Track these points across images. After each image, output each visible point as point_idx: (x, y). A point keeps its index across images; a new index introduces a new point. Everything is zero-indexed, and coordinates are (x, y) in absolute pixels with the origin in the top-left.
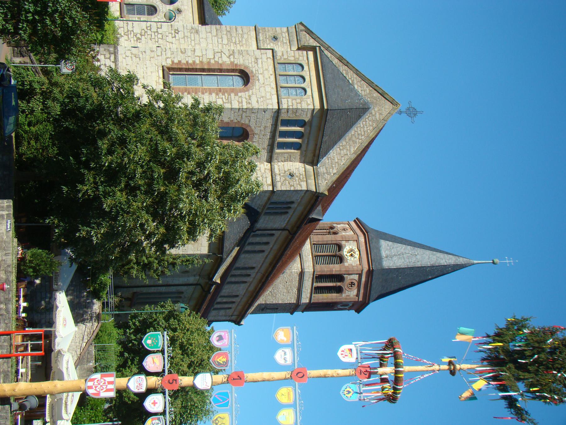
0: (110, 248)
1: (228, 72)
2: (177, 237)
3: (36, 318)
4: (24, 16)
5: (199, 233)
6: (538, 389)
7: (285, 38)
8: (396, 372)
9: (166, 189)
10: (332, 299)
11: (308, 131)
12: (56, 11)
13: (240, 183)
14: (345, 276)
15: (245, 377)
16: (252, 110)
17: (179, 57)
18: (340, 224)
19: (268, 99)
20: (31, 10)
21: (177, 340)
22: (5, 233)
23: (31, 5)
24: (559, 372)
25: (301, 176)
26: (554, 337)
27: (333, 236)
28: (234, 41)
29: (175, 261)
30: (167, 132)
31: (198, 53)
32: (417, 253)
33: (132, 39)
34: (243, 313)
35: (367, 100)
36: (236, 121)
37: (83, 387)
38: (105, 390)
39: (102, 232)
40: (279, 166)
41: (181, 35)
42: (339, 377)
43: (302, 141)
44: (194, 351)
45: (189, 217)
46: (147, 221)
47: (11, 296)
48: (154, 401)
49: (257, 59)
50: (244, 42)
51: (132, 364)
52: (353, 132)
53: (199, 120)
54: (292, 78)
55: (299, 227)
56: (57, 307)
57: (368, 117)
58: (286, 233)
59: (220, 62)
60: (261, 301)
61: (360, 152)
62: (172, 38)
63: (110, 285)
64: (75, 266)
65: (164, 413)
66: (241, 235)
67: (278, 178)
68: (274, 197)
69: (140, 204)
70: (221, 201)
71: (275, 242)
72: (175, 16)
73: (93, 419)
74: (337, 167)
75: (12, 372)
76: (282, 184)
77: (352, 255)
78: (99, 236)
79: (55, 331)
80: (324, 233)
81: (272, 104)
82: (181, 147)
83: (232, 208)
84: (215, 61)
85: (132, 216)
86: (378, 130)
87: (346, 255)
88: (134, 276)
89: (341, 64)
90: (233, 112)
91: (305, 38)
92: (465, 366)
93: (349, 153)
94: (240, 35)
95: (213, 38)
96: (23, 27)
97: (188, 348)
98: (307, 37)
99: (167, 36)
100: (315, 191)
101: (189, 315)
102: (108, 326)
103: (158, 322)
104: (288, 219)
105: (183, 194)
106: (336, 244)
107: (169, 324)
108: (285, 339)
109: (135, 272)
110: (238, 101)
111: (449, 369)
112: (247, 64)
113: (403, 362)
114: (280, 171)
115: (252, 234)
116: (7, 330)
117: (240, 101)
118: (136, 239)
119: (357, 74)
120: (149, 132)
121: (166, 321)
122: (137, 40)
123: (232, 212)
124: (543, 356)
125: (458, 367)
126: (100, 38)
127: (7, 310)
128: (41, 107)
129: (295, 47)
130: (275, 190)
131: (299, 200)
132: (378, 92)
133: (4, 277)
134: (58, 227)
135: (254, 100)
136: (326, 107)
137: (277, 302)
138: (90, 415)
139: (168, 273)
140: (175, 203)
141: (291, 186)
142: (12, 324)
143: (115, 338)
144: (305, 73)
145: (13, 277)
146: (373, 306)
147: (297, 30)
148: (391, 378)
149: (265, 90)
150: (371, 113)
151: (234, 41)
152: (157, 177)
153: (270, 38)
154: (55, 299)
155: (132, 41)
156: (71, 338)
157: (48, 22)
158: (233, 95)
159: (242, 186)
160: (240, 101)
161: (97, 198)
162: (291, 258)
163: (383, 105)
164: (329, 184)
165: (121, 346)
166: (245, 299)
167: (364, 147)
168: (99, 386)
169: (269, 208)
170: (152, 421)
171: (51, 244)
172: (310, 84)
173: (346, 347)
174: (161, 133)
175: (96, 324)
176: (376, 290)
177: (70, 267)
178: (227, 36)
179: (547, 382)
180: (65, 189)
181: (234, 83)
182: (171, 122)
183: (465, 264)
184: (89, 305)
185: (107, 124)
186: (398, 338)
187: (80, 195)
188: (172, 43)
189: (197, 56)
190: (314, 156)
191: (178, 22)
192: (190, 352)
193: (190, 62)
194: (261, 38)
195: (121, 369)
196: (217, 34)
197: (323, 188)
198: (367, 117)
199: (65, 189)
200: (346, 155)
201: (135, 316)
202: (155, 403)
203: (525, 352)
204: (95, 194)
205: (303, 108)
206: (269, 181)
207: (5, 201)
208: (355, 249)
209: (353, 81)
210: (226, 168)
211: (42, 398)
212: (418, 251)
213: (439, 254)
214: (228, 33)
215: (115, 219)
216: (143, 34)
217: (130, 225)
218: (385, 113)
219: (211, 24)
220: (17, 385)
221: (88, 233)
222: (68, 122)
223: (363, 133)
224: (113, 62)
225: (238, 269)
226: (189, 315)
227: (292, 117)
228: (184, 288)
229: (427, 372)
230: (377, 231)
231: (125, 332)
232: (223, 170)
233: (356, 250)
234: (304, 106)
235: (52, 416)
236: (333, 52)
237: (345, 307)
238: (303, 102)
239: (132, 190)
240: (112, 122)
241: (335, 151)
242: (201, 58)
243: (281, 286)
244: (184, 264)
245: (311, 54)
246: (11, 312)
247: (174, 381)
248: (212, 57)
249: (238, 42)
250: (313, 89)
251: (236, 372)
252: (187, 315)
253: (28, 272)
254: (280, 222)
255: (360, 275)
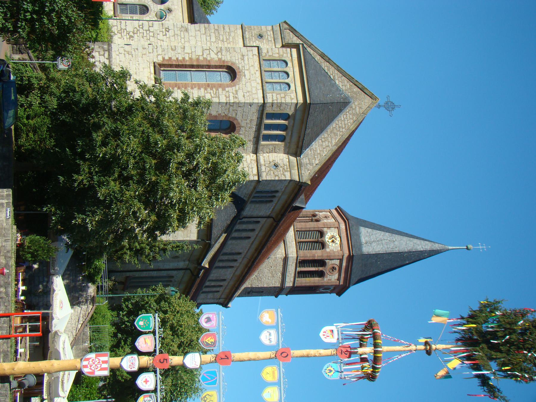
0: (104, 235)
1: (216, 68)
2: (168, 224)
3: (34, 300)
4: (22, 15)
5: (189, 220)
6: (509, 368)
7: (270, 36)
8: (375, 352)
9: (158, 179)
10: (315, 283)
11: (292, 124)
12: (53, 10)
13: (227, 173)
14: (327, 261)
15: (232, 357)
16: (239, 104)
17: (169, 54)
18: (322, 212)
19: (254, 94)
20: (30, 10)
21: (167, 322)
22: (4, 220)
23: (29, 5)
24: (529, 352)
25: (286, 167)
26: (525, 319)
27: (316, 223)
28: (221, 39)
29: (166, 247)
30: (158, 125)
31: (187, 50)
32: (394, 240)
33: (125, 37)
34: (230, 296)
35: (348, 95)
36: (223, 114)
37: (79, 366)
38: (99, 368)
39: (97, 219)
40: (264, 157)
41: (171, 33)
42: (321, 356)
43: (286, 134)
44: (184, 332)
45: (179, 206)
46: (139, 209)
47: (10, 280)
48: (146, 379)
49: (243, 56)
50: (231, 40)
51: (125, 344)
52: (334, 125)
53: (189, 114)
54: (277, 74)
55: (283, 215)
56: (54, 291)
57: (349, 111)
58: (271, 220)
59: (208, 59)
60: (247, 284)
61: (340, 144)
62: (163, 35)
63: (104, 270)
64: (71, 252)
65: (155, 391)
66: (229, 222)
67: (263, 168)
68: (260, 186)
69: (132, 193)
70: (210, 190)
71: (261, 229)
72: (166, 15)
73: (88, 396)
74: (319, 158)
75: (11, 352)
76: (267, 174)
77: (333, 241)
78: (94, 223)
79: (52, 313)
80: (307, 221)
81: (258, 99)
82: (171, 139)
83: (220, 196)
84: (204, 58)
85: (125, 204)
86: (358, 123)
87: (328, 241)
88: (127, 261)
89: (323, 61)
90: (220, 106)
91: (289, 36)
92: (440, 346)
93: (330, 145)
94: (227, 33)
95: (202, 36)
96: (22, 25)
97: (178, 329)
98: (291, 35)
99: (158, 34)
100: (298, 180)
101: (179, 298)
102: (102, 308)
103: (150, 305)
104: (273, 207)
105: (173, 184)
106: (319, 231)
107: (160, 306)
108: (270, 321)
109: (128, 258)
110: (226, 96)
111: (426, 349)
112: (234, 61)
113: (381, 342)
114: (265, 162)
115: (239, 221)
116: (7, 312)
117: (227, 95)
118: (128, 226)
119: (338, 70)
120: (141, 125)
121: (157, 304)
122: (130, 38)
123: (220, 200)
124: (514, 336)
125: (434, 347)
126: (94, 36)
127: (7, 294)
128: (39, 101)
129: (279, 45)
130: (260, 180)
131: (283, 189)
132: (358, 87)
133: (4, 262)
134: (55, 214)
135: (240, 94)
136: (308, 102)
137: (262, 286)
138: (85, 393)
139: (159, 258)
140: (166, 192)
141: (276, 176)
142: (12, 307)
143: (109, 320)
144: (289, 69)
145: (12, 262)
146: (353, 290)
147: (281, 28)
148: (371, 357)
149: (251, 85)
150: (352, 107)
151: (221, 39)
152: (149, 168)
153: (256, 36)
154: (52, 283)
155: (125, 39)
156: (68, 320)
157: (46, 21)
158: (220, 90)
159: (229, 176)
160: (227, 95)
161: (91, 187)
162: (276, 244)
163: (363, 99)
164: (311, 174)
165: (114, 327)
166: (232, 283)
167: (344, 139)
168: (94, 365)
169: (254, 197)
170: (144, 398)
171: (49, 231)
172: (293, 80)
173: (327, 328)
174: (153, 126)
175: (91, 306)
176: (356, 274)
177: (67, 252)
178: (215, 34)
179: (518, 362)
180: (61, 178)
181: (222, 79)
182: (162, 116)
183: (440, 250)
184: (84, 289)
185: (101, 118)
186: (377, 320)
187: (76, 185)
188: (163, 41)
189: (187, 53)
190: (298, 147)
191: (169, 20)
192: (180, 333)
193: (180, 58)
194: (247, 36)
195: (115, 349)
196: (205, 32)
197: (306, 177)
198: (348, 110)
199: (61, 178)
200: (327, 146)
201: (128, 299)
202: (146, 381)
203: (497, 333)
204: (90, 184)
205: (287, 102)
206: (255, 171)
207: (5, 190)
208: (336, 235)
209: (334, 77)
210: (214, 159)
211: (40, 376)
212: (396, 238)
213: (415, 241)
214: (216, 31)
215: (109, 207)
216: (136, 32)
217: (123, 213)
218: (364, 107)
219: (200, 23)
220: (16, 365)
221: (84, 220)
222: (65, 115)
223: (344, 126)
224: (107, 58)
225: (226, 254)
226: (179, 298)
227: (276, 110)
228: (174, 273)
229: (404, 352)
230: (357, 218)
231: (118, 314)
232: (211, 161)
233: (338, 236)
234: (288, 100)
235: (49, 394)
236: (315, 49)
237: (327, 291)
238: (287, 97)
239: (125, 180)
240: (106, 115)
241: (317, 143)
242: (190, 54)
243: (266, 271)
244: (174, 249)
245: (294, 51)
246: (11, 295)
247: (165, 361)
248: (201, 54)
249: (225, 40)
250: (296, 84)
251: (223, 352)
252: (177, 298)
253: (26, 258)
254: (265, 210)
255: (341, 260)
